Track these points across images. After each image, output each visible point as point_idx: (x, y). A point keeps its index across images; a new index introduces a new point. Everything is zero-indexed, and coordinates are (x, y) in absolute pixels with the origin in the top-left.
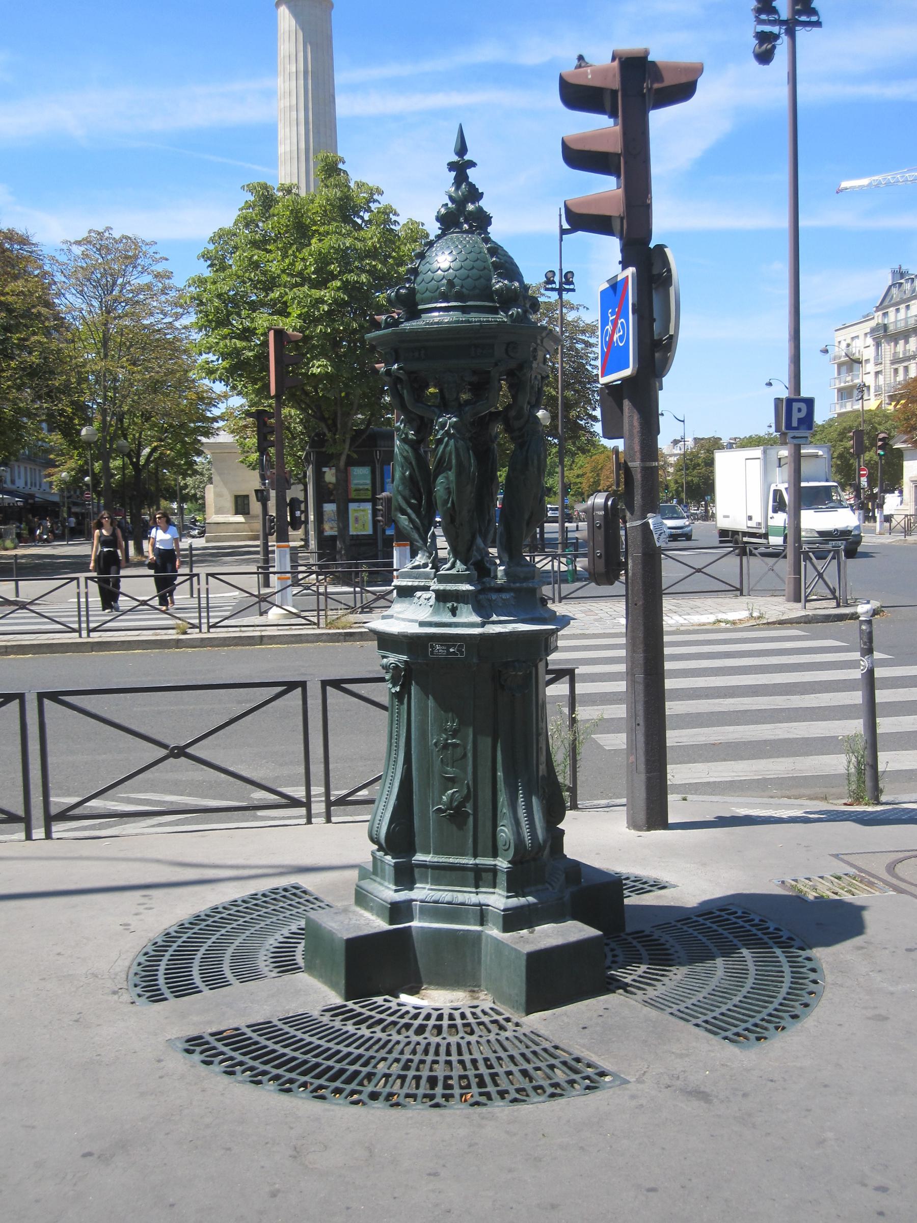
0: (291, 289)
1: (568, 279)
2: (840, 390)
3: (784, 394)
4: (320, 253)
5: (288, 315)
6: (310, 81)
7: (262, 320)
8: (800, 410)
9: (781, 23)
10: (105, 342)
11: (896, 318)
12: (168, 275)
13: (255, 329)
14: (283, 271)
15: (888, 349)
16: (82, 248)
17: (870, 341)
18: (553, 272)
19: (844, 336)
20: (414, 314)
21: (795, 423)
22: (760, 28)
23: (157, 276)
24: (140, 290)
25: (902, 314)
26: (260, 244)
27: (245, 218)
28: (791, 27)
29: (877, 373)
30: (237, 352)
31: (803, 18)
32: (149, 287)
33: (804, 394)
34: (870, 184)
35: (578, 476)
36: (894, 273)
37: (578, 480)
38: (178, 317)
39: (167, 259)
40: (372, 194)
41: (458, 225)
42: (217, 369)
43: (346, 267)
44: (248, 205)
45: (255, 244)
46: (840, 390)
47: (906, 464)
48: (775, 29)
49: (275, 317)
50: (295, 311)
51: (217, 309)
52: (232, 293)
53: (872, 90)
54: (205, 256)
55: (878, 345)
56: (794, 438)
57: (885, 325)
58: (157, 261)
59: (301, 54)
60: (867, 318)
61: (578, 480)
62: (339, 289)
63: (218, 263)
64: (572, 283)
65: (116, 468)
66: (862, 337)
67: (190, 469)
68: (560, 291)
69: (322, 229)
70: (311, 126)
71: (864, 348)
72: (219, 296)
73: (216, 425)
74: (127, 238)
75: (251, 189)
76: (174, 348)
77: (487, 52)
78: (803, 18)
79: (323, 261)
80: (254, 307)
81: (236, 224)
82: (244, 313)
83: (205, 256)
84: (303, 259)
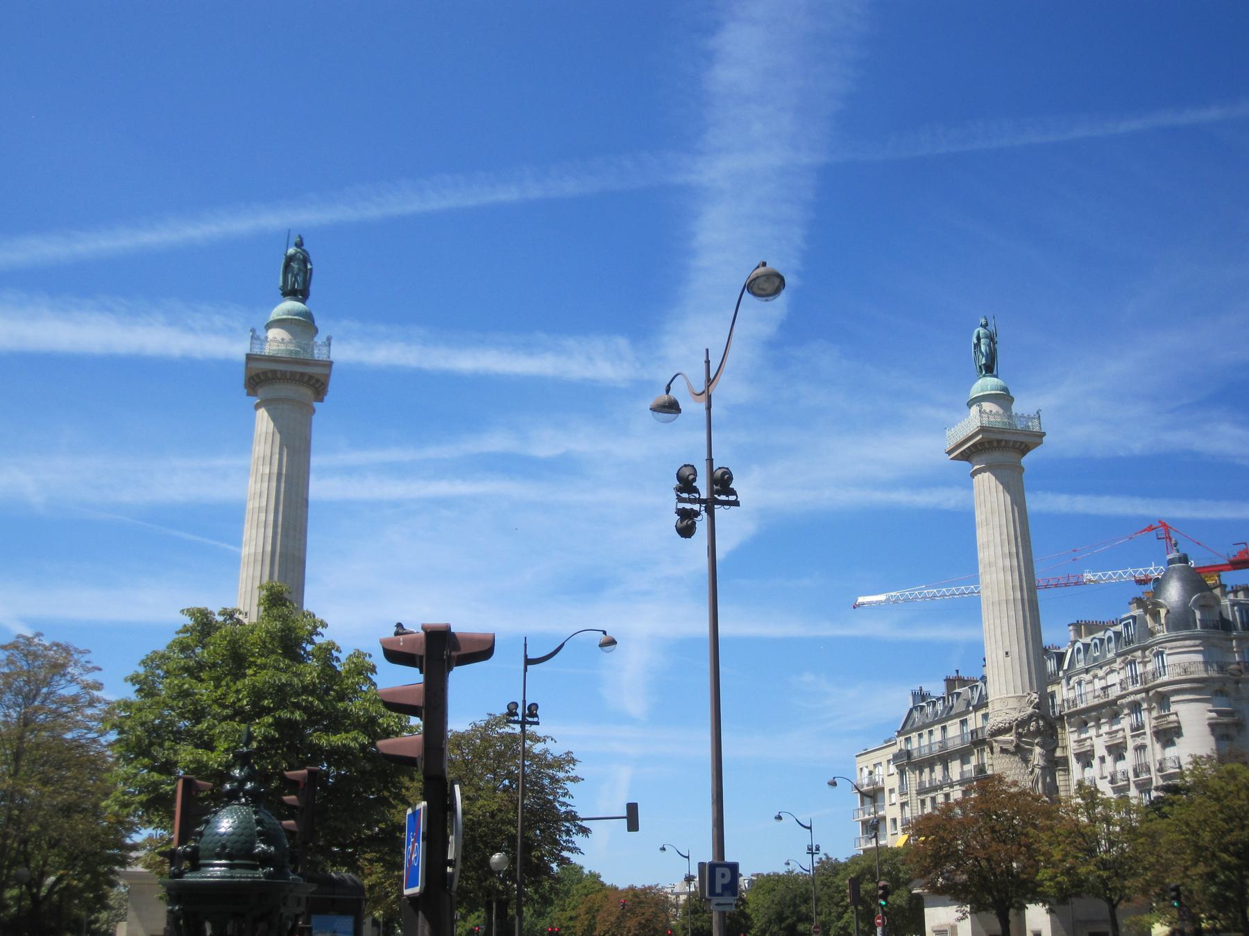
0: (220, 722)
1: (532, 711)
2: (864, 823)
3: (708, 857)
4: (254, 686)
5: (212, 749)
6: (283, 485)
7: (186, 754)
8: (723, 876)
9: (700, 501)
10: (17, 757)
11: (921, 744)
12: (98, 686)
13: (177, 762)
14: (215, 701)
15: (912, 778)
16: (7, 653)
17: (893, 769)
18: (516, 704)
19: (866, 762)
20: (196, 867)
21: (718, 890)
22: (681, 506)
23: (87, 687)
24: (63, 701)
25: (925, 741)
26: (194, 672)
27: (181, 643)
28: (710, 505)
29: (903, 805)
30: (156, 785)
31: (723, 498)
32: (75, 699)
33: (729, 858)
34: (888, 600)
35: (571, 919)
36: (914, 695)
37: (571, 923)
38: (102, 733)
39: (100, 669)
40: (315, 627)
41: (238, 799)
42: (132, 803)
43: (281, 703)
44: (185, 629)
45: (187, 669)
46: (864, 823)
47: (928, 911)
48: (696, 507)
49: (200, 751)
50: (222, 745)
51: (139, 739)
52: (157, 722)
53: (902, 497)
54: (134, 679)
55: (902, 773)
56: (718, 904)
57: (908, 751)
58: (89, 671)
59: (276, 457)
60: (889, 743)
61: (571, 923)
62: (270, 725)
63: (146, 687)
64: (536, 716)
65: (11, 898)
66: (885, 764)
67: (101, 902)
68: (523, 723)
69: (259, 661)
70: (279, 530)
71: (888, 777)
72: (143, 724)
73: (133, 854)
74: (58, 645)
75: (191, 613)
76: (95, 766)
77: (497, 442)
78: (723, 498)
79: (257, 694)
80: (178, 736)
81: (170, 647)
82: (167, 744)
83: (134, 679)
84: (238, 691)
